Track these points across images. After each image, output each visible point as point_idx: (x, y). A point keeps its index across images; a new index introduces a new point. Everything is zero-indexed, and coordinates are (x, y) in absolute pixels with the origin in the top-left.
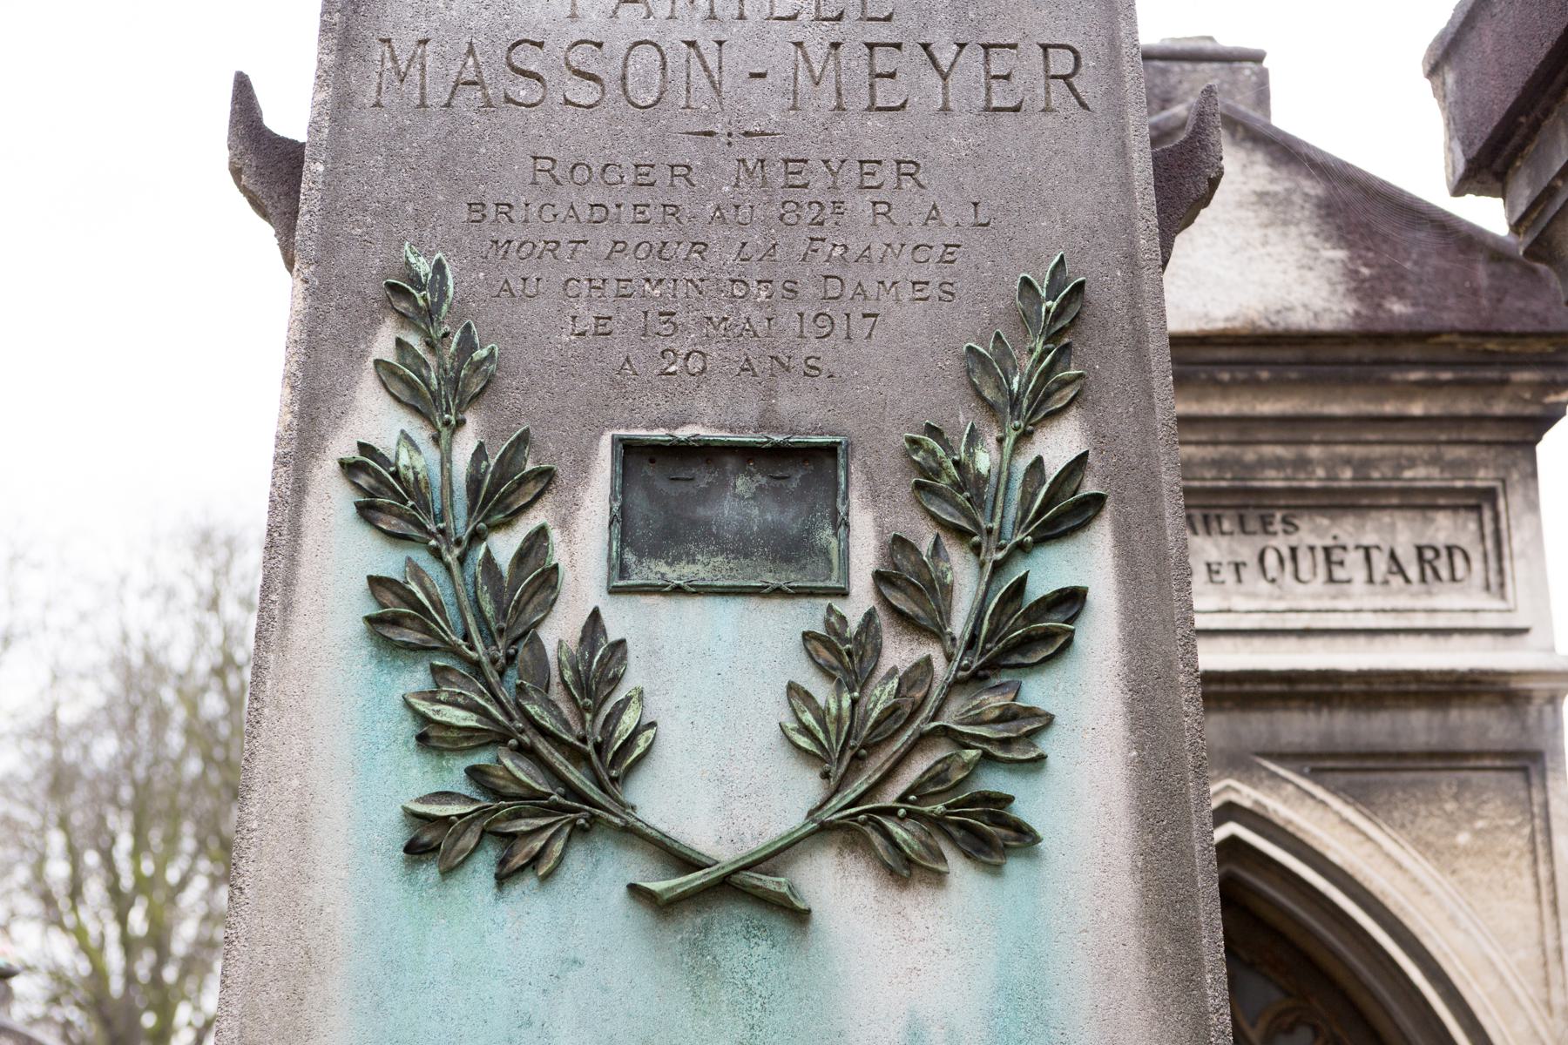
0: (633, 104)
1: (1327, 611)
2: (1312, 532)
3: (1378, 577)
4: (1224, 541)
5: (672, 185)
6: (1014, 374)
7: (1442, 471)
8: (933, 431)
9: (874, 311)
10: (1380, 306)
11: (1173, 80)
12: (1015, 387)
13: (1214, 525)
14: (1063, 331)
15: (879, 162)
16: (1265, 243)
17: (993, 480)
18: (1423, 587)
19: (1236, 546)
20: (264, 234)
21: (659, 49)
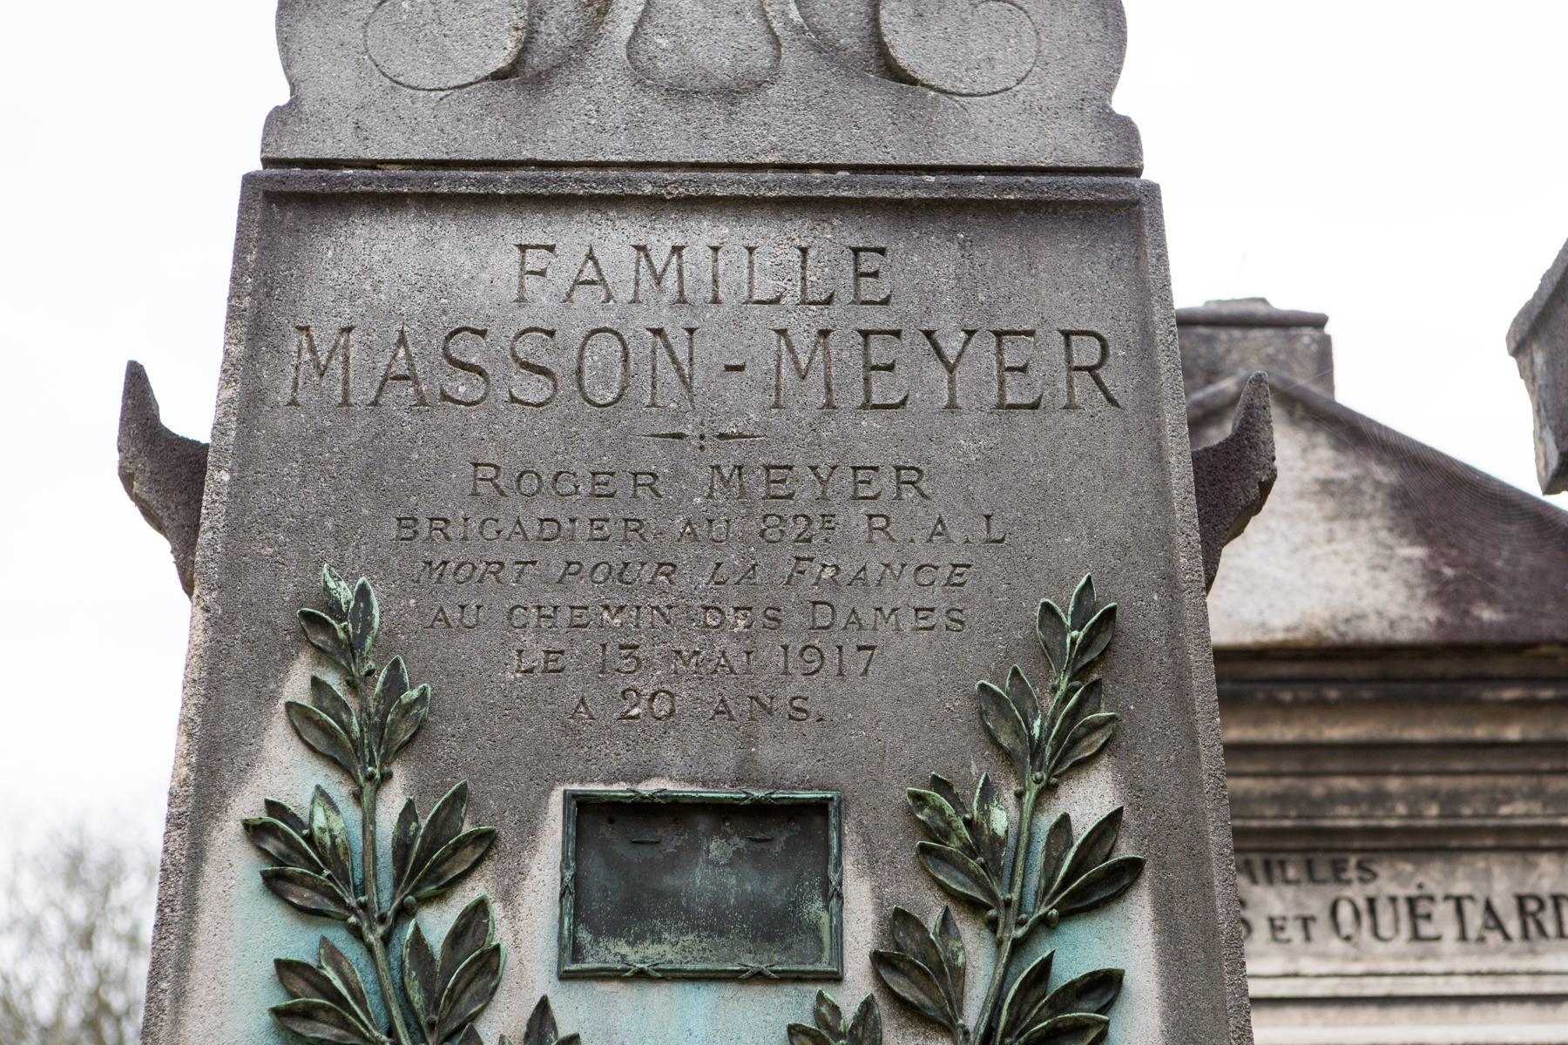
0: (589, 401)
1: (1413, 974)
2: (1393, 881)
3: (1472, 933)
4: (1289, 892)
5: (635, 496)
6: (1035, 717)
7: (1545, 806)
8: (940, 785)
9: (870, 642)
10: (1466, 613)
11: (1220, 349)
12: (1036, 732)
13: (1277, 872)
14: (1091, 666)
15: (875, 469)
16: (1330, 540)
17: (1011, 841)
18: (1525, 945)
19: (1303, 897)
20: (159, 548)
21: (621, 338)
